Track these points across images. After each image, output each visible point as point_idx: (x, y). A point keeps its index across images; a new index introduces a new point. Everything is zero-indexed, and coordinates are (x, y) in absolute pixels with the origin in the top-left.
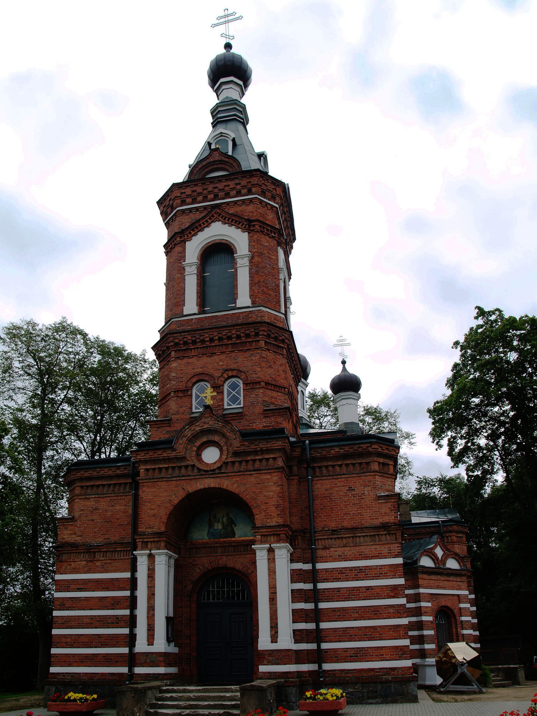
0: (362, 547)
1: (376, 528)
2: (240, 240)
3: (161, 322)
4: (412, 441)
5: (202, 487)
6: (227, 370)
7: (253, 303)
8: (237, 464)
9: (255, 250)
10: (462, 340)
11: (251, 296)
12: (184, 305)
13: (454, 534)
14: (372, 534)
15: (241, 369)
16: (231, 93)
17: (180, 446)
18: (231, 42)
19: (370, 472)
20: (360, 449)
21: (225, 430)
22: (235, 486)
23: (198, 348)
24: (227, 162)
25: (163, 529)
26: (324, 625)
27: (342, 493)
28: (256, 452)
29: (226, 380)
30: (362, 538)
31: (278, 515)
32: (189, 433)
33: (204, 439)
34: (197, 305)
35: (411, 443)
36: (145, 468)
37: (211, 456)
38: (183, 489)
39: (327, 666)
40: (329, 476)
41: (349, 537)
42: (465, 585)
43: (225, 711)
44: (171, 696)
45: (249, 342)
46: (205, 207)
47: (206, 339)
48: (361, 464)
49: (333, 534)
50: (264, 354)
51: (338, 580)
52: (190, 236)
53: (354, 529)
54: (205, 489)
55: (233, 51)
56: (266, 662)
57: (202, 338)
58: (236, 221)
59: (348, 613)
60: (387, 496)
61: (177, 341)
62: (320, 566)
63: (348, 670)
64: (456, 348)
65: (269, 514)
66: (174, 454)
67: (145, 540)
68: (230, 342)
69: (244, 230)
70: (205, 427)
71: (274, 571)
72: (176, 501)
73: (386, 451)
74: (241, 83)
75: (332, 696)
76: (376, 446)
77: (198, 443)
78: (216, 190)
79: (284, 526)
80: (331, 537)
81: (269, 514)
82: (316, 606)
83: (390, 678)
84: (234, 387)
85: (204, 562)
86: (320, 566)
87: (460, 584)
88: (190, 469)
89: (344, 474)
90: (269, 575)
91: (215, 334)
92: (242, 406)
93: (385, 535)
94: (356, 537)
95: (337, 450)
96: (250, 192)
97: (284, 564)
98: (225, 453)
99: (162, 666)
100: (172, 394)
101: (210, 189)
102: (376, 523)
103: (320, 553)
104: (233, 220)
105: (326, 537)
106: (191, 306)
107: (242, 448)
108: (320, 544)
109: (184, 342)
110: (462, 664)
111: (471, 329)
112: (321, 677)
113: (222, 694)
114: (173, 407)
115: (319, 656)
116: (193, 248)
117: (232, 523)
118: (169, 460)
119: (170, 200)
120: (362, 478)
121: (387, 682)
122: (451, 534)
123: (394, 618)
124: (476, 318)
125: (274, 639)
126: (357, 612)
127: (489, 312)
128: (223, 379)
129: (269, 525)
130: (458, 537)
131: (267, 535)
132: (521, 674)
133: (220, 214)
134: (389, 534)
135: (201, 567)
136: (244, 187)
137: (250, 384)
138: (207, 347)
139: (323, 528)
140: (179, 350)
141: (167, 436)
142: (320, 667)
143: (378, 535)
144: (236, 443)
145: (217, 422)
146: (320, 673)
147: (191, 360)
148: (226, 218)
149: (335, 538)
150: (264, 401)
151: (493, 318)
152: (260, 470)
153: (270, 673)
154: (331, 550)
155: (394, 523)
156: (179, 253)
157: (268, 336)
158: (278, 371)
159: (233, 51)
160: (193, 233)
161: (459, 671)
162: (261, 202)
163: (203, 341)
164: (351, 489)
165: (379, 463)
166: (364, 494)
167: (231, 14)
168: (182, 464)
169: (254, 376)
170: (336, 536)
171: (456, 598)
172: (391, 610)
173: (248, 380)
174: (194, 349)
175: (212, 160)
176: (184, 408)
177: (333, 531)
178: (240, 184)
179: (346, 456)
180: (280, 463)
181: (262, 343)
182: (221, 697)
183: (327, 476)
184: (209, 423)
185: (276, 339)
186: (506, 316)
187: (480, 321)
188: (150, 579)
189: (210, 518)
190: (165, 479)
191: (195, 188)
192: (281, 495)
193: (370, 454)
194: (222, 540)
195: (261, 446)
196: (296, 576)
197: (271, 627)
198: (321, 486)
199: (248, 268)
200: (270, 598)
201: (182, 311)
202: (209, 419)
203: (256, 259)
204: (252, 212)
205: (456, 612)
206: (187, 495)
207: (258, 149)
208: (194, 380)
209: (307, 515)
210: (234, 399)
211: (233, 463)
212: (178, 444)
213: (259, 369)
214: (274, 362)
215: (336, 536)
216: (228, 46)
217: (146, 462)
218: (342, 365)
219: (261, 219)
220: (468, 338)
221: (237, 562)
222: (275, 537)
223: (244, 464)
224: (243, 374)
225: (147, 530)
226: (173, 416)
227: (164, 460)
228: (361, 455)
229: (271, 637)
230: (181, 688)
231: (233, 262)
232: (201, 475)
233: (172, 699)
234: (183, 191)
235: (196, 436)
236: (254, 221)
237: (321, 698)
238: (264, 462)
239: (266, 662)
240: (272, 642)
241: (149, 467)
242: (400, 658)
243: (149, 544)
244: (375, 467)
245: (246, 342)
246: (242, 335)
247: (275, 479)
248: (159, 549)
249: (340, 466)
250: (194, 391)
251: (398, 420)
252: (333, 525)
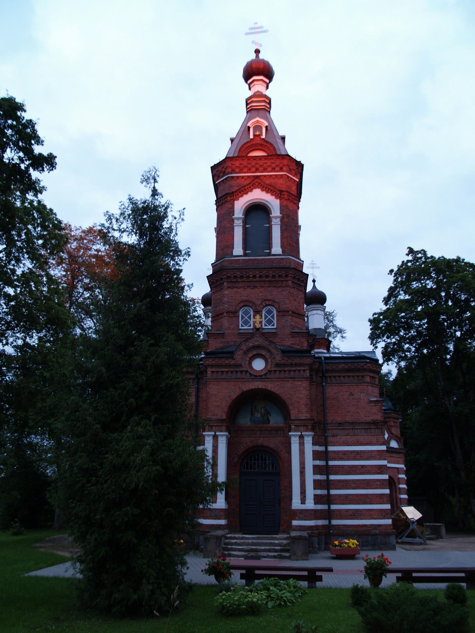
0: (359, 437)
1: (369, 423)
2: (274, 203)
3: (212, 258)
4: (344, 335)
5: (253, 388)
6: (265, 300)
7: (283, 251)
8: (277, 373)
9: (284, 213)
10: (396, 269)
11: (282, 247)
12: (233, 248)
13: (392, 420)
14: (366, 427)
15: (275, 300)
16: (259, 87)
17: (238, 356)
18: (260, 49)
19: (365, 383)
20: (359, 366)
21: (270, 347)
22: (277, 388)
23: (244, 282)
24: (266, 146)
25: (224, 417)
26: (333, 492)
27: (345, 397)
28: (291, 365)
29: (264, 307)
30: (359, 430)
31: (307, 411)
32: (244, 347)
33: (255, 352)
34: (243, 248)
35: (343, 337)
36: (211, 370)
37: (259, 365)
38: (239, 388)
39: (334, 522)
40: (337, 384)
41: (350, 429)
42: (402, 460)
43: (279, 553)
44: (236, 542)
45: (281, 281)
46: (248, 177)
47: (250, 276)
48: (358, 376)
49: (339, 426)
50: (292, 290)
51: (342, 459)
52: (238, 196)
53: (353, 423)
54: (255, 389)
55: (261, 56)
56: (297, 518)
57: (247, 274)
58: (272, 190)
59: (348, 483)
60: (376, 401)
61: (229, 275)
62: (331, 448)
63: (349, 525)
64: (391, 274)
65: (300, 411)
66: (233, 362)
67: (211, 424)
68: (267, 279)
69: (277, 198)
70: (256, 344)
71: (302, 452)
72: (234, 397)
73: (375, 368)
74: (268, 81)
75: (353, 545)
76: (370, 365)
77: (250, 355)
78: (257, 166)
79: (310, 420)
80: (338, 428)
81: (300, 411)
82: (328, 477)
83: (377, 532)
84: (269, 312)
85: (247, 441)
86: (331, 448)
87: (399, 459)
88: (244, 373)
89: (347, 383)
90: (300, 455)
91: (257, 273)
92: (275, 327)
93: (374, 428)
94: (355, 429)
95: (343, 365)
96: (281, 170)
97: (309, 448)
98: (270, 363)
99: (223, 519)
100: (225, 314)
101: (253, 164)
102: (369, 419)
103: (330, 439)
104: (269, 189)
105: (334, 428)
106: (238, 250)
107: (282, 361)
108: (330, 433)
109: (234, 276)
110: (413, 522)
111: (403, 262)
112: (331, 530)
113: (272, 541)
114: (226, 324)
115: (329, 514)
116: (240, 205)
117: (268, 413)
118: (230, 366)
119: (223, 168)
120: (360, 386)
121: (376, 535)
122: (389, 420)
123: (380, 488)
124: (408, 255)
125: (303, 501)
126: (355, 483)
127: (417, 251)
128: (262, 306)
129: (300, 418)
130: (394, 422)
131: (299, 426)
132: (443, 530)
133: (260, 183)
134: (377, 428)
135: (245, 445)
136: (277, 166)
137: (281, 311)
138: (250, 281)
139: (332, 421)
140: (230, 282)
141: (221, 345)
142: (330, 522)
143: (370, 428)
144: (278, 357)
145: (264, 341)
146: (329, 526)
147: (238, 290)
148: (264, 187)
149: (340, 429)
150: (291, 325)
151: (420, 255)
152: (295, 378)
153: (300, 526)
154: (338, 437)
155: (381, 420)
156: (229, 208)
157: (294, 278)
158: (299, 303)
159: (261, 56)
160: (240, 195)
161: (411, 527)
162: (288, 177)
163: (248, 277)
164: (351, 394)
165: (370, 376)
166: (360, 398)
167: (260, 28)
168: (239, 370)
169: (284, 306)
170: (341, 428)
171: (396, 470)
172: (378, 483)
173: (280, 308)
174: (241, 282)
175: (254, 143)
176: (234, 326)
177: (340, 423)
178: (274, 163)
179: (348, 370)
180: (308, 374)
181: (290, 283)
182: (272, 543)
183: (335, 384)
184: (258, 341)
185: (298, 279)
186: (429, 255)
187: (410, 258)
188: (214, 454)
189: (252, 408)
190: (226, 380)
191: (242, 162)
192: (308, 397)
193: (364, 370)
194: (260, 425)
195: (296, 361)
196: (316, 456)
197: (301, 493)
198: (331, 391)
199: (280, 226)
200: (300, 472)
201: (232, 252)
202: (259, 338)
203: (286, 220)
204: (282, 184)
205: (396, 480)
206: (242, 393)
207: (281, 133)
208: (241, 305)
209: (321, 411)
210: (270, 322)
211: (275, 371)
212: (236, 355)
213: (288, 302)
214: (297, 297)
215: (341, 428)
216: (257, 52)
217: (212, 366)
218: (313, 283)
219: (288, 190)
220: (399, 268)
221: (272, 442)
222: (305, 427)
223: (282, 372)
224: (276, 304)
225: (213, 417)
226: (225, 331)
227: (226, 366)
228: (359, 370)
229: (301, 500)
230: (233, 535)
231: (269, 221)
232: (253, 379)
233: (236, 544)
234: (233, 163)
235: (249, 350)
236: (284, 191)
237: (346, 546)
238: (297, 372)
239: (297, 518)
240: (302, 503)
241: (214, 370)
242: (384, 518)
243: (214, 428)
244: (368, 379)
245: (279, 281)
246: (276, 275)
247: (305, 385)
248: (221, 431)
249: (344, 377)
250: (241, 313)
251: (335, 318)
252: (339, 419)
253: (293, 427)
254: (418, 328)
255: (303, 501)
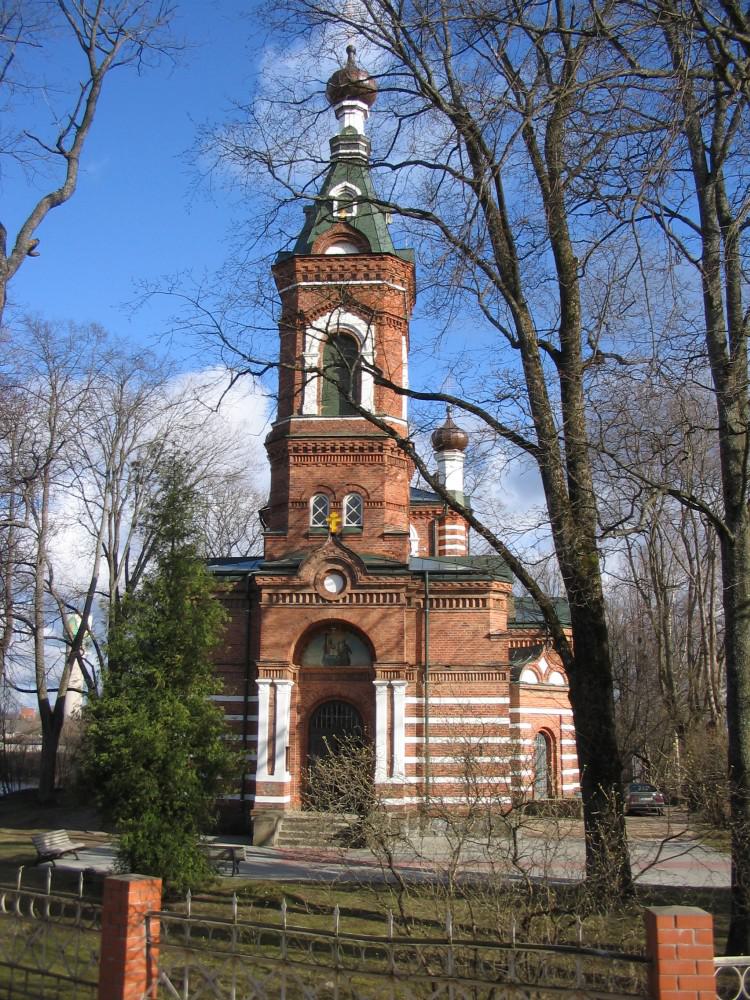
125: (391, 773)
163: (306, 450)
253: (379, 673)
254: (339, 962)
255: (391, 773)
